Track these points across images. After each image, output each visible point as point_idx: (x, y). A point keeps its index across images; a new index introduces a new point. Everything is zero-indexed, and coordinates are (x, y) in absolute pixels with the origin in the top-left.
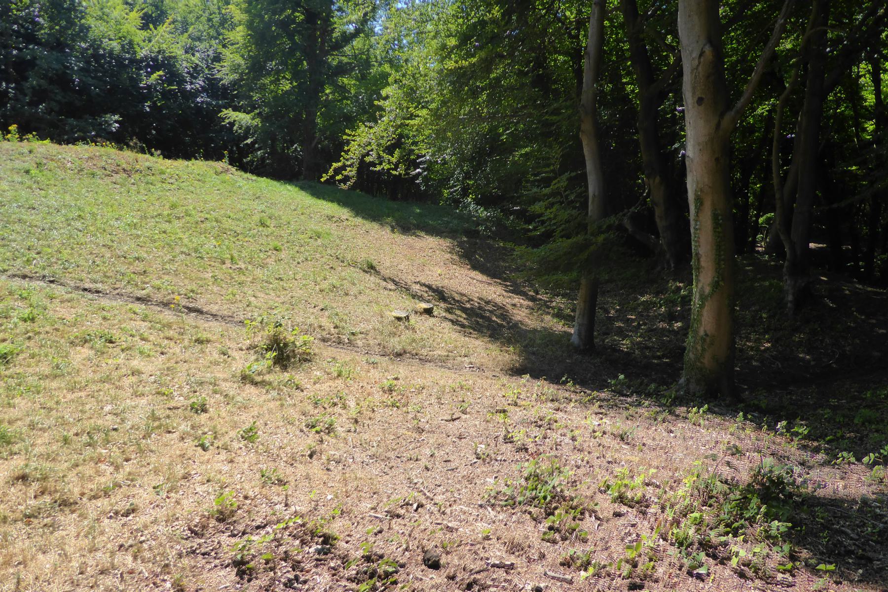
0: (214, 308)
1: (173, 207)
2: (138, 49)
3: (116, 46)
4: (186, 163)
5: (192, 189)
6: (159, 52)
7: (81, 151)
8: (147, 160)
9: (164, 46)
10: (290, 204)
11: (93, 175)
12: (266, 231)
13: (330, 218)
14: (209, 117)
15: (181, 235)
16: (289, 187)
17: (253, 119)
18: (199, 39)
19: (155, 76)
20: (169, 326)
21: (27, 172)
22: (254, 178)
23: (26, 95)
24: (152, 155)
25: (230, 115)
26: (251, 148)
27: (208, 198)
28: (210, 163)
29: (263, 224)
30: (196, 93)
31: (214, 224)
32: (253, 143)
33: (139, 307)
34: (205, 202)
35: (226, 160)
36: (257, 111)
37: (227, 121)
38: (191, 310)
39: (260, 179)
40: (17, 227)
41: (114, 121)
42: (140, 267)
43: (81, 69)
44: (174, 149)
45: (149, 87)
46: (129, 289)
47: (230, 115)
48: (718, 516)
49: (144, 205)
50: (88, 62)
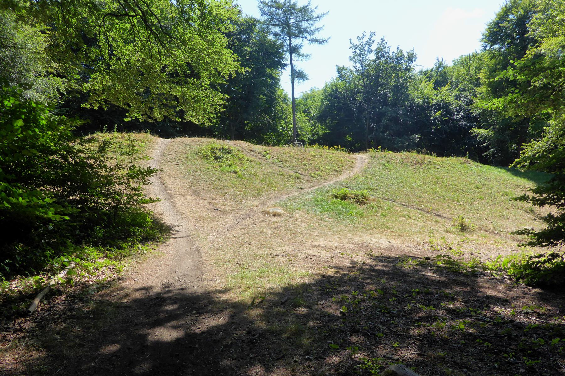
0: (445, 215)
1: (437, 179)
2: (431, 100)
3: (421, 100)
4: (447, 159)
5: (447, 171)
6: (442, 100)
7: (402, 156)
8: (429, 158)
9: (444, 98)
10: (497, 179)
11: (407, 165)
12: (478, 191)
13: (518, 186)
14: (466, 131)
15: (438, 190)
16: (500, 170)
17: (488, 132)
18: (464, 90)
19: (437, 114)
20: (428, 217)
21: (384, 165)
22: (481, 165)
23: (380, 128)
24: (432, 155)
25: (476, 131)
26: (487, 148)
27: (454, 175)
28: (459, 158)
29: (478, 188)
30: (459, 120)
31: (454, 186)
32: (488, 146)
33: (419, 211)
34: (452, 177)
35: (467, 156)
36: (492, 128)
37: (474, 134)
38: (436, 215)
39: (485, 166)
40: (383, 184)
41: (416, 137)
42: (421, 200)
43: (404, 114)
44: (443, 150)
45: (435, 119)
46: (416, 206)
47: (476, 131)
48: (305, 111)
49: (425, 178)
50: (407, 111)
